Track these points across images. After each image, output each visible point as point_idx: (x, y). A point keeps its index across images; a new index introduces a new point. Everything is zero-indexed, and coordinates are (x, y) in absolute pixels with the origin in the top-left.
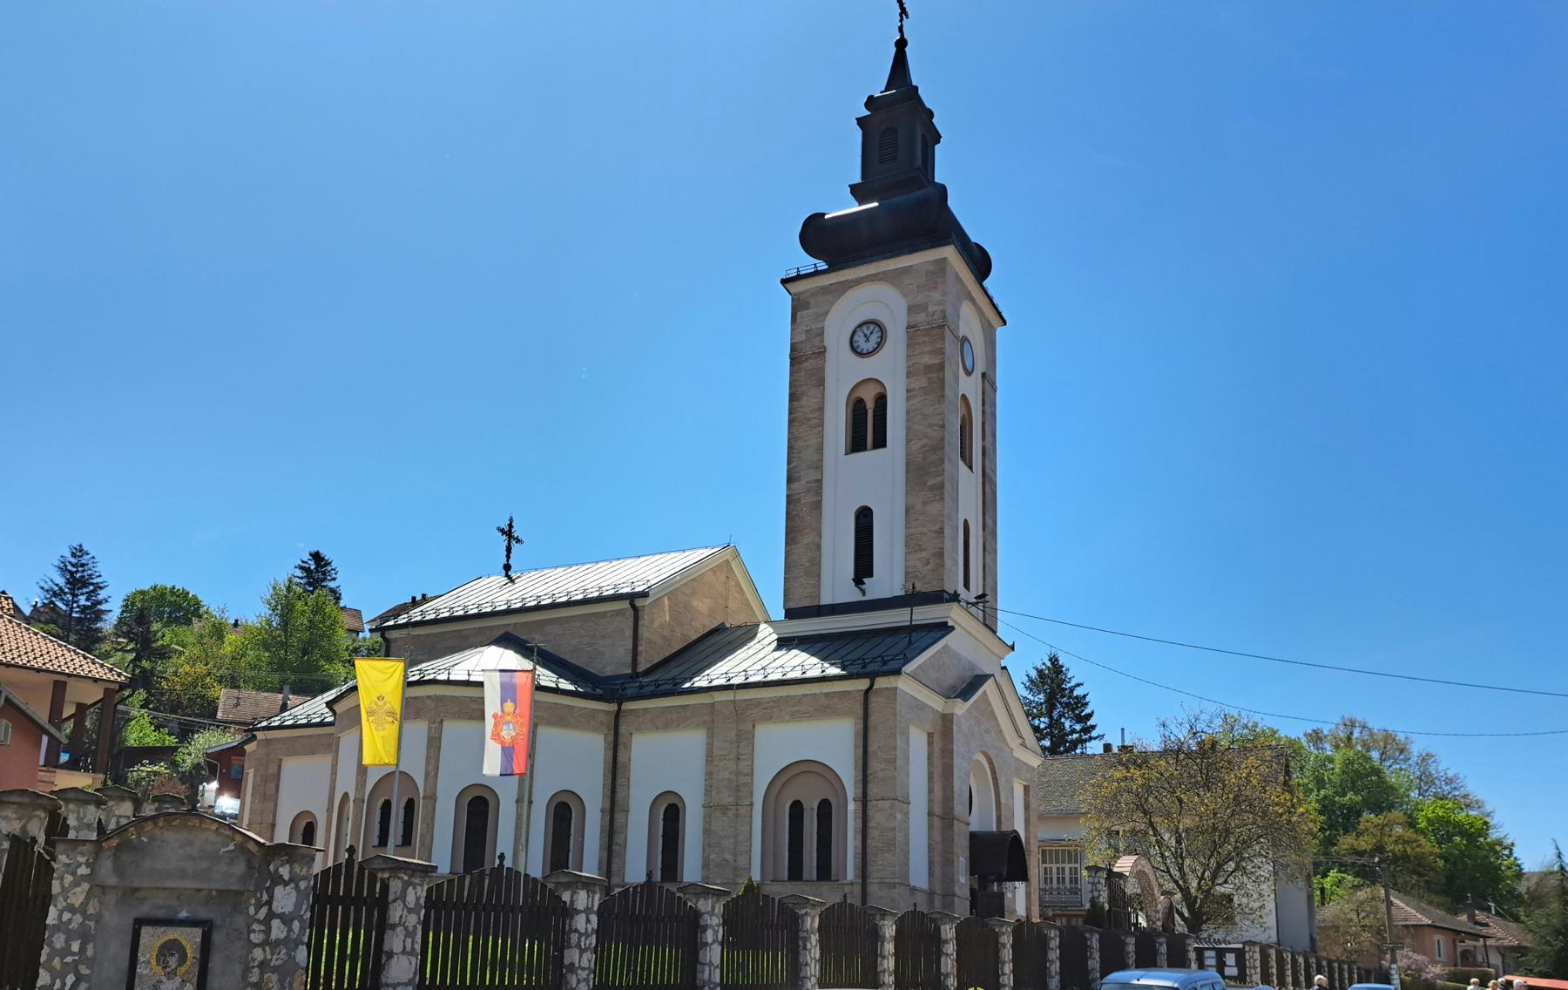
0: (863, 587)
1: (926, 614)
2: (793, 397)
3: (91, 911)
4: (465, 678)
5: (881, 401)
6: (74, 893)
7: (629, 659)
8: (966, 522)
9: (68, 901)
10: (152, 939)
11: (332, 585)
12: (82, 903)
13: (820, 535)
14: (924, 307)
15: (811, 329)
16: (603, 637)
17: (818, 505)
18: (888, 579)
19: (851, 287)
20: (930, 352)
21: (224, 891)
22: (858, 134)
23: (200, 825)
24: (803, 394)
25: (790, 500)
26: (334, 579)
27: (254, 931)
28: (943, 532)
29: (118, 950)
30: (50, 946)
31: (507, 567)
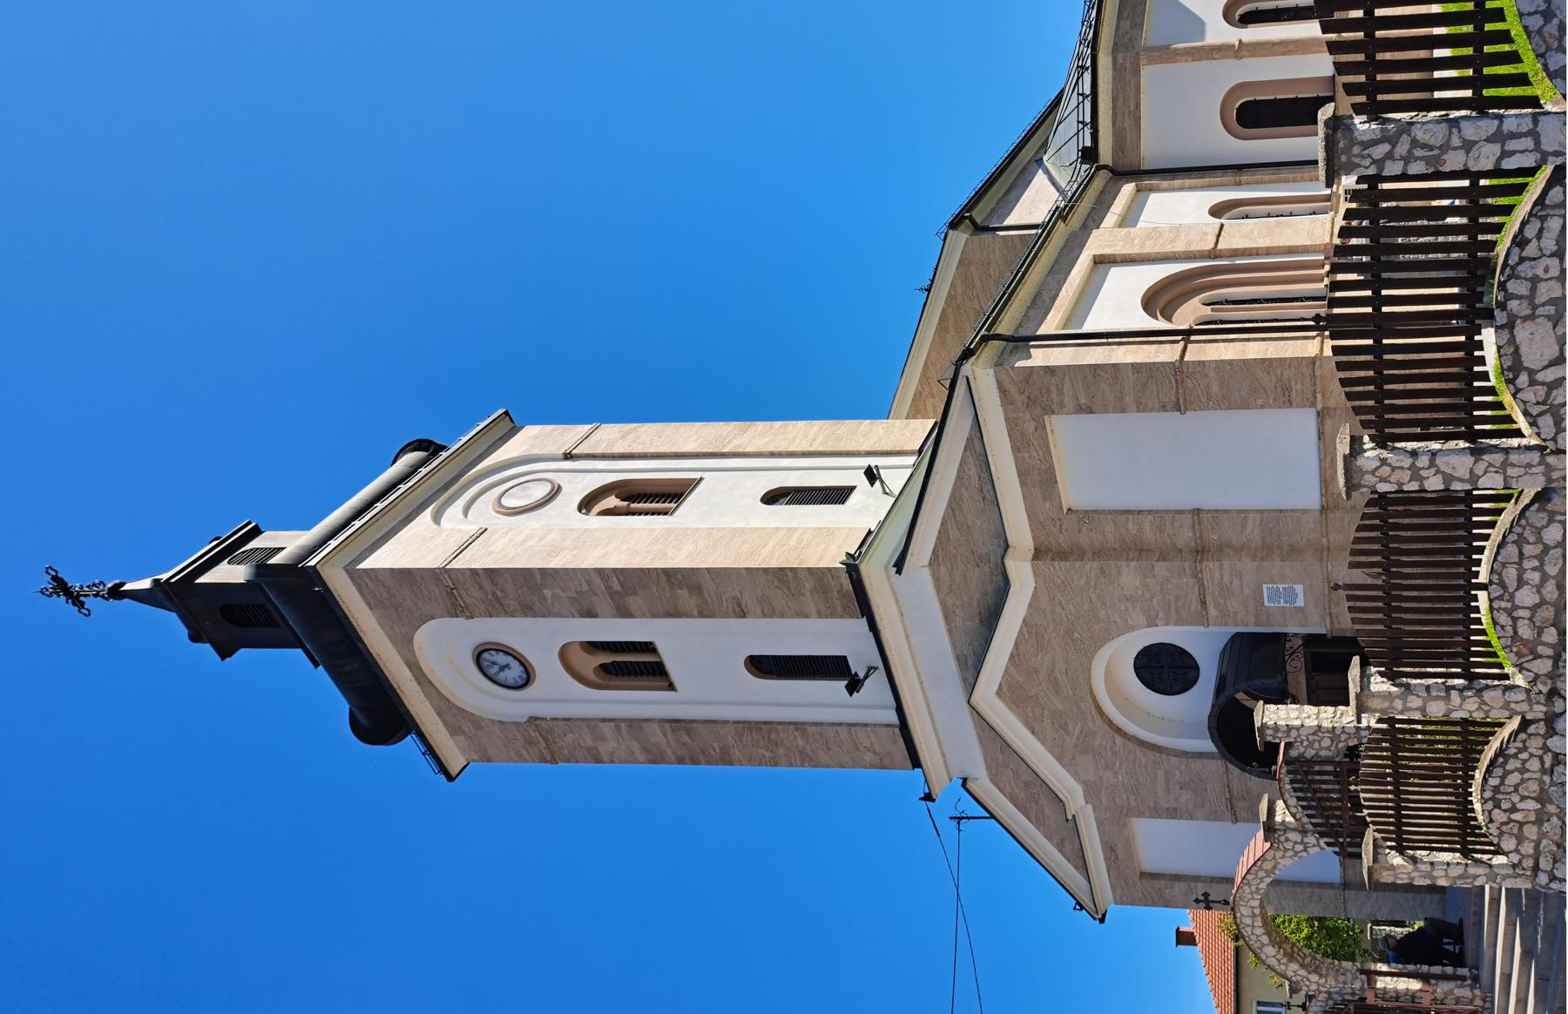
8: (772, 498)
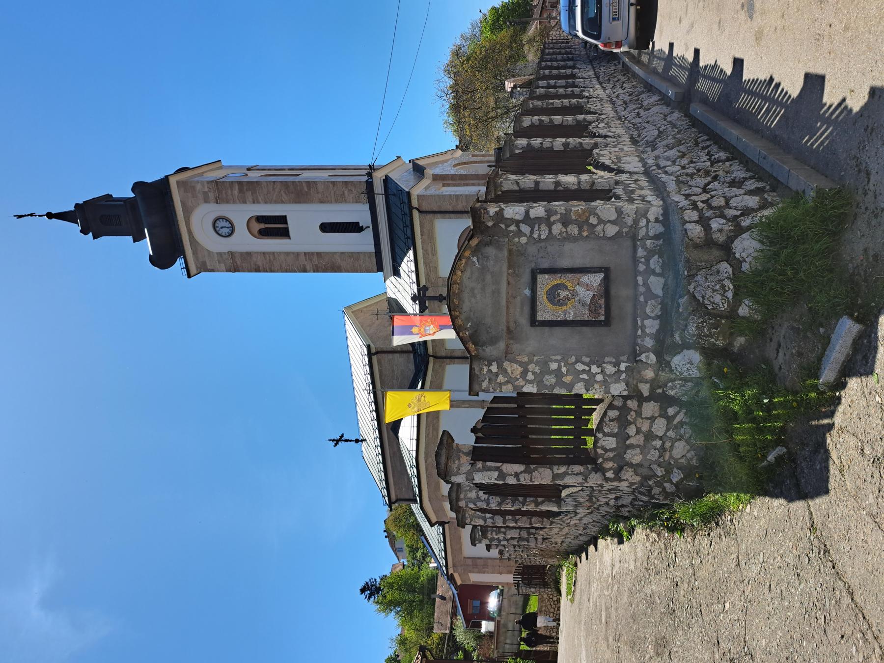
0: (364, 227)
1: (379, 188)
2: (257, 270)
3: (526, 359)
4: (415, 442)
5: (260, 219)
6: (512, 373)
7: (405, 355)
9: (518, 377)
10: (546, 311)
11: (378, 580)
12: (519, 366)
13: (335, 253)
14: (205, 193)
15: (218, 260)
16: (393, 371)
17: (319, 255)
18: (359, 213)
19: (193, 237)
20: (232, 190)
21: (509, 262)
23: (458, 284)
24: (255, 264)
25: (316, 270)
26: (375, 580)
27: (539, 235)
28: (334, 182)
29: (557, 336)
30: (553, 387)
31: (357, 441)
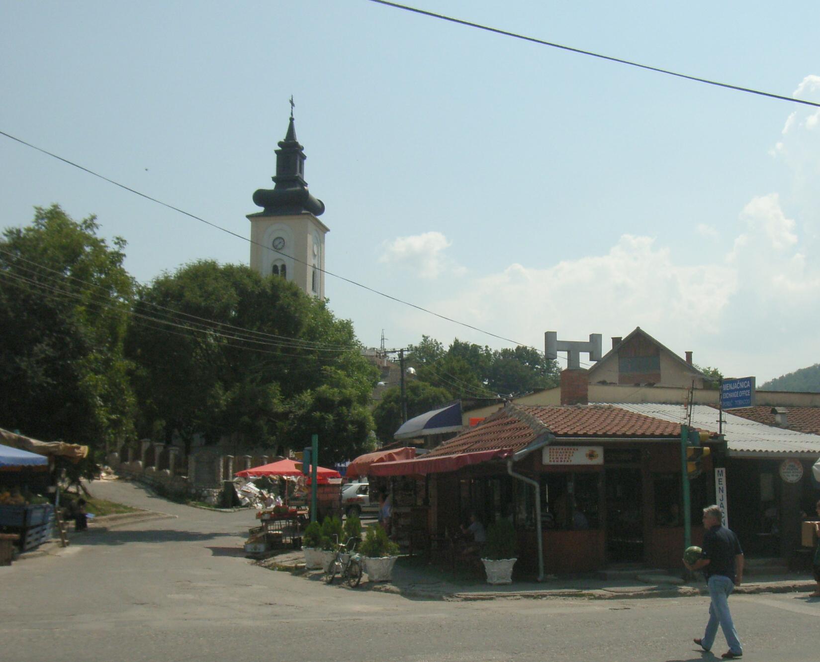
22: (275, 156)
